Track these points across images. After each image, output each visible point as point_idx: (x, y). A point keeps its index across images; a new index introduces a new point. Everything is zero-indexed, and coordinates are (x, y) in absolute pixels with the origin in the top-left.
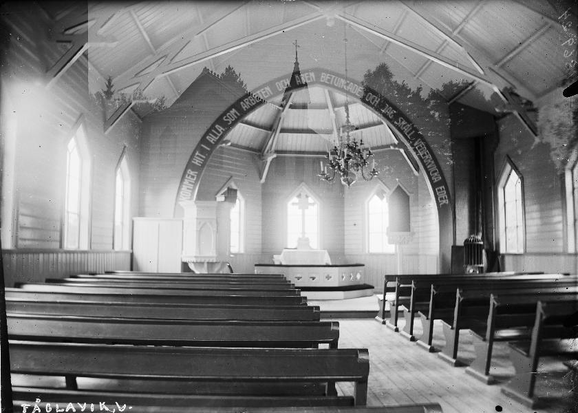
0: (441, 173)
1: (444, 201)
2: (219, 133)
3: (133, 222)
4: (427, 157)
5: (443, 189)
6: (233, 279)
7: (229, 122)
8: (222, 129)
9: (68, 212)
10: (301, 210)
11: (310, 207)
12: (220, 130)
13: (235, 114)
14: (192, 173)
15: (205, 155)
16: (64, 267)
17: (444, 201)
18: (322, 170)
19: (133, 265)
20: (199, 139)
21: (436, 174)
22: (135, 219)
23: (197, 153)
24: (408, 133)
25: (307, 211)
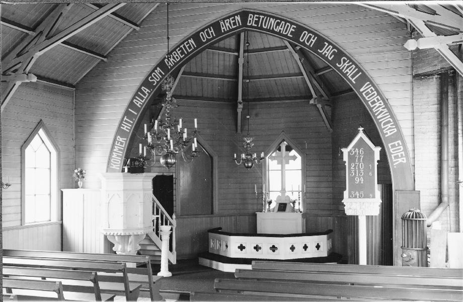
0: (396, 124)
1: (400, 160)
2: (145, 95)
3: (62, 192)
4: (377, 104)
5: (399, 145)
6: (370, 232)
7: (154, 82)
8: (147, 90)
9: (387, 100)
10: (280, 165)
11: (291, 161)
12: (146, 92)
13: (160, 73)
14: (121, 140)
15: (132, 121)
16: (323, 185)
17: (400, 160)
18: (141, 152)
19: (64, 244)
20: (126, 104)
21: (389, 126)
22: (65, 191)
23: (125, 119)
24: (353, 77)
25: (287, 166)
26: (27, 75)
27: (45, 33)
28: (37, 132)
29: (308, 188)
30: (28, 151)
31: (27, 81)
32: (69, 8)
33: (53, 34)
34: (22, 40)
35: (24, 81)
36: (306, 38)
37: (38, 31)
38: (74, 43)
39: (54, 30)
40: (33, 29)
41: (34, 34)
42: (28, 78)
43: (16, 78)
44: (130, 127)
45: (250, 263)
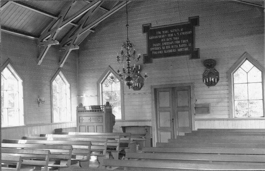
26: (54, 41)
27: (63, 18)
28: (58, 73)
29: (98, 132)
30: (54, 83)
31: (54, 44)
32: (74, 4)
33: (67, 18)
34: (50, 22)
35: (52, 45)
36: (163, 40)
37: (59, 16)
38: (104, 6)
39: (66, 17)
40: (56, 15)
41: (56, 18)
42: (54, 43)
43: (49, 43)
44: (159, 46)
45: (44, 167)
